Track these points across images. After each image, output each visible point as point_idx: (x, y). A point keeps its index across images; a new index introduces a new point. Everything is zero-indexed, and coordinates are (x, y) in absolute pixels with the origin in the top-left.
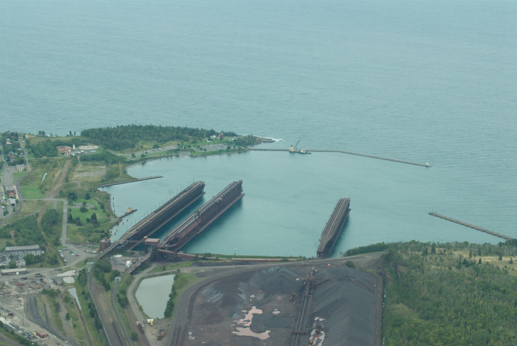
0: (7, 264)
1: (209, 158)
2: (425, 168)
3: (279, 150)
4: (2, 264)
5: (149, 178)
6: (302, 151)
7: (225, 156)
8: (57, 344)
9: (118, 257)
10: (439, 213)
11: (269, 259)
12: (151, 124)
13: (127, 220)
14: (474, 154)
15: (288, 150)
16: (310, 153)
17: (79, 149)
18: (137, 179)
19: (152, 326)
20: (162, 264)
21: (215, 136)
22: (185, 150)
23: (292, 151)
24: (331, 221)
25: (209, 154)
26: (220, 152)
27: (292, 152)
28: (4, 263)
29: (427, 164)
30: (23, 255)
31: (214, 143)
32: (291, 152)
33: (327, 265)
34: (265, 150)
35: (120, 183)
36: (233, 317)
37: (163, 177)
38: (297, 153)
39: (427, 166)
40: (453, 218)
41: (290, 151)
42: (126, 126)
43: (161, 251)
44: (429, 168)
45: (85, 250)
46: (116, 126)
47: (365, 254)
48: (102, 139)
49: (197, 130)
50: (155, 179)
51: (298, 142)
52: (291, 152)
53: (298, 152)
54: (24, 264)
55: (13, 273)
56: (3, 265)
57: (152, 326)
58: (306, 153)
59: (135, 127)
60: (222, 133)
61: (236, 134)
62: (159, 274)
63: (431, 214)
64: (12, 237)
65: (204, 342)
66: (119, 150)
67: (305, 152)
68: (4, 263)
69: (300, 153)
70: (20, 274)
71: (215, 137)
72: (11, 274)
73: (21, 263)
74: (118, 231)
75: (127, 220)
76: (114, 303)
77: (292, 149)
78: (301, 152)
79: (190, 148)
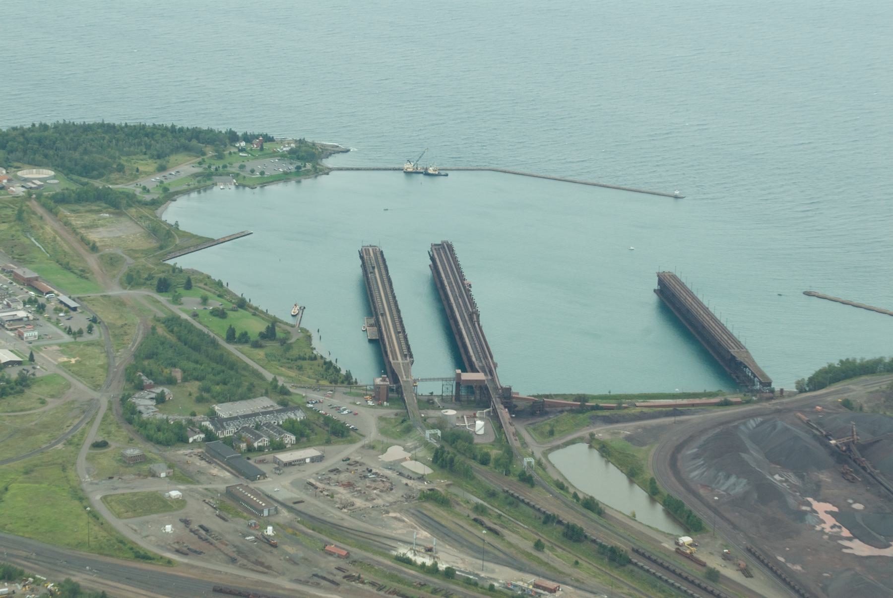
2: (672, 199)
5: (234, 237)
6: (431, 171)
7: (292, 185)
8: (144, 539)
11: (704, 400)
12: (103, 121)
13: (318, 331)
14: (793, 173)
16: (447, 175)
17: (17, 175)
18: (213, 240)
21: (244, 143)
25: (272, 182)
26: (285, 177)
27: (411, 173)
29: (677, 192)
31: (253, 157)
32: (408, 173)
33: (815, 408)
34: (358, 169)
37: (252, 233)
38: (421, 175)
39: (676, 197)
40: (867, 303)
41: (405, 170)
42: (120, 126)
43: (552, 402)
44: (679, 200)
46: (207, 128)
48: (58, 155)
49: (143, 127)
50: (246, 237)
52: (408, 173)
53: (422, 173)
54: (293, 439)
55: (300, 461)
56: (259, 444)
58: (439, 175)
59: (109, 128)
63: (808, 294)
66: (100, 176)
67: (437, 173)
69: (427, 174)
70: (313, 462)
75: (318, 331)
77: (409, 167)
78: (430, 172)
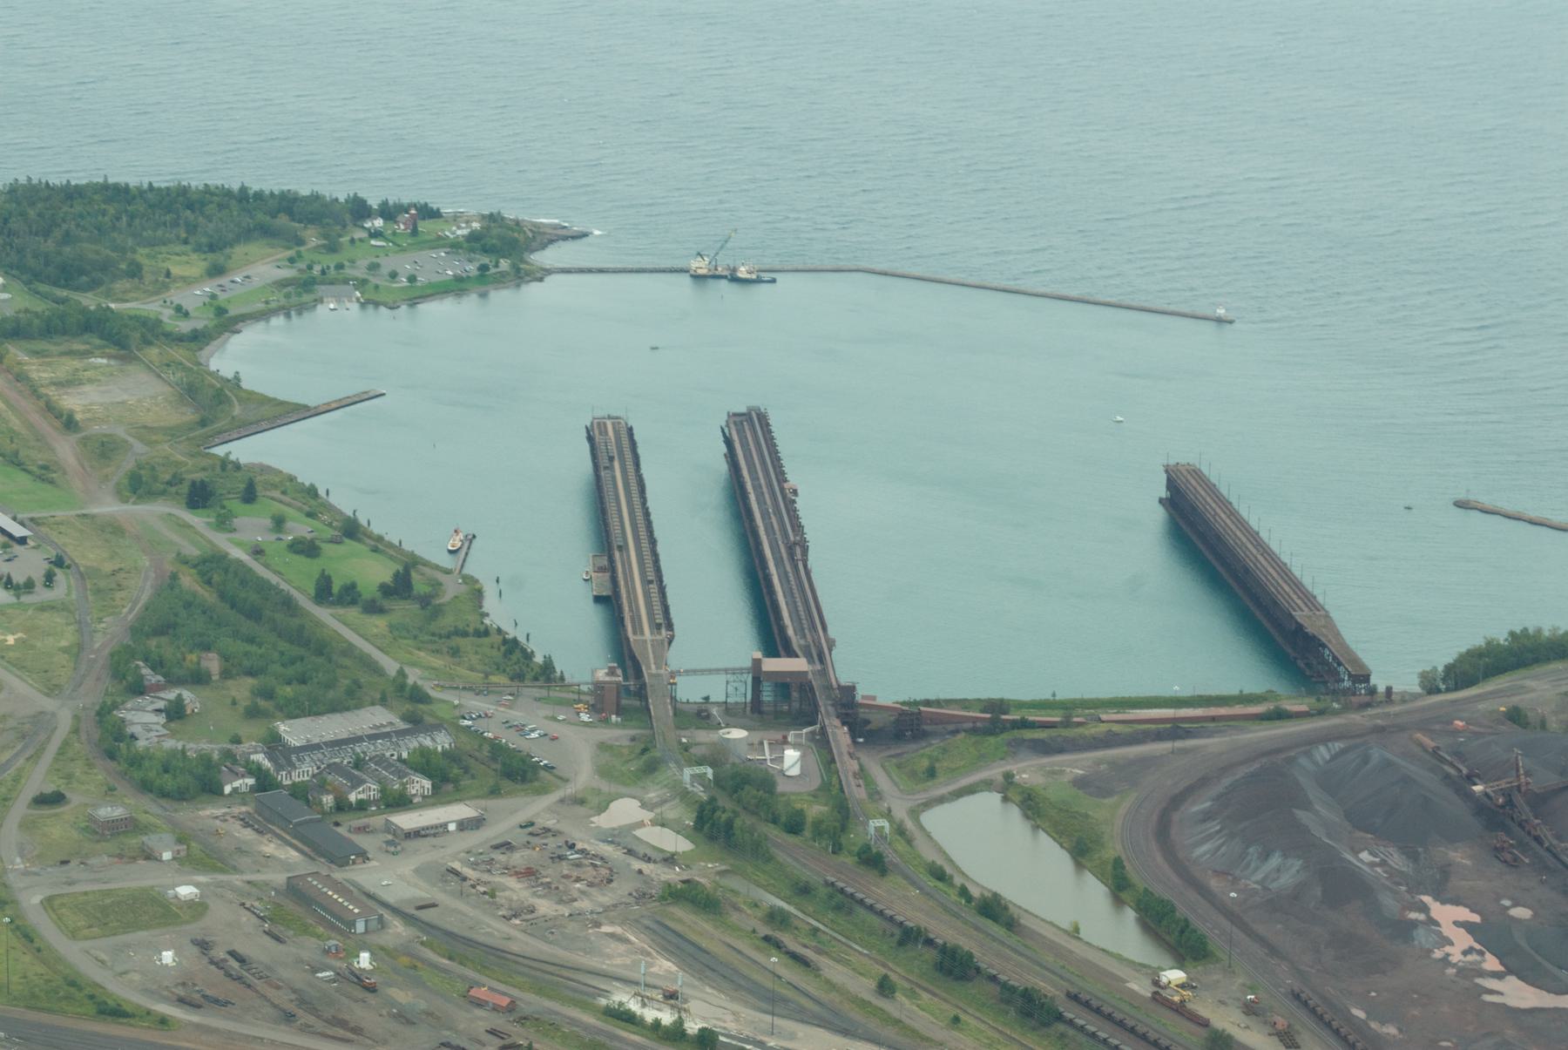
0: (372, 793)
1: (426, 308)
2: (1209, 327)
3: (631, 271)
4: (354, 793)
7: (471, 302)
9: (735, 740)
10: (1486, 500)
11: (1238, 710)
15: (687, 271)
18: (306, 408)
19: (381, 1015)
20: (892, 752)
22: (325, 279)
23: (700, 272)
24: (1273, 559)
27: (704, 277)
28: (361, 789)
29: (1221, 312)
30: (395, 753)
33: (1452, 723)
35: (264, 425)
36: (1416, 942)
39: (1220, 321)
41: (692, 273)
45: (550, 713)
47: (1523, 672)
51: (719, 245)
52: (697, 278)
54: (426, 786)
55: (437, 827)
56: (361, 796)
57: (381, 1015)
58: (759, 281)
60: (413, 212)
61: (438, 209)
62: (950, 793)
63: (1461, 505)
64: (214, 678)
65: (1449, 1041)
66: (93, 285)
68: (363, 791)
69: (734, 279)
70: (461, 830)
71: (382, 224)
72: (432, 832)
73: (417, 786)
74: (518, 627)
76: (971, 920)
77: (700, 266)
78: (740, 275)
79: (341, 271)
